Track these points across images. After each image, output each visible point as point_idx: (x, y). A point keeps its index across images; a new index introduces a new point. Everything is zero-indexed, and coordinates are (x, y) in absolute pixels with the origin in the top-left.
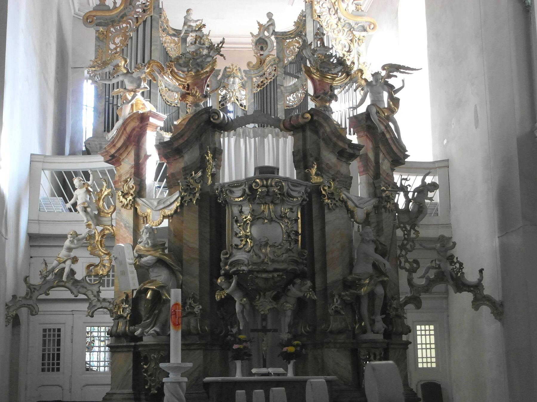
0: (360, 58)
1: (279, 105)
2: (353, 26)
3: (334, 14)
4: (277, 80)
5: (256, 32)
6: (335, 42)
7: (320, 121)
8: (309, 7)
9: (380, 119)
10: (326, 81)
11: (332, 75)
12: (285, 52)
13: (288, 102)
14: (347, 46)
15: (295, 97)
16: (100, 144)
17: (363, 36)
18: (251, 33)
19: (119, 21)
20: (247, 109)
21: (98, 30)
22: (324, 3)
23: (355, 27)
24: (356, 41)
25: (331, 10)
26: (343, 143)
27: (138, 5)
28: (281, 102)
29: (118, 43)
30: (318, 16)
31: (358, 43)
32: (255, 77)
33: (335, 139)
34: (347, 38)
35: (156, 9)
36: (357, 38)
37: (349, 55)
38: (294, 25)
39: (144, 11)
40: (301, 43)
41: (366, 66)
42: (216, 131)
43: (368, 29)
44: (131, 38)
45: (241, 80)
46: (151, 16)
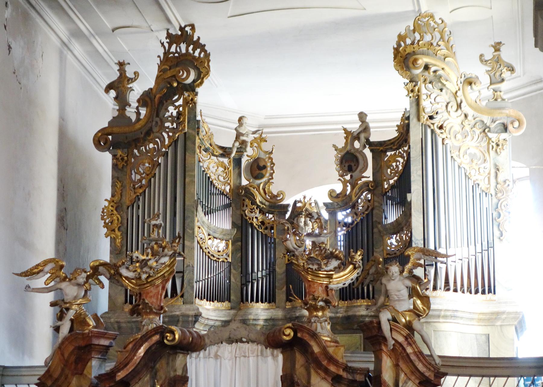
1: (376, 252)
2: (488, 125)
3: (457, 110)
4: (374, 215)
5: (341, 144)
6: (457, 153)
7: (305, 338)
8: (414, 105)
10: (319, 282)
11: (325, 273)
12: (385, 171)
13: (389, 248)
16: (117, 322)
17: (504, 140)
18: (334, 146)
19: (144, 140)
21: (116, 154)
22: (438, 95)
23: (491, 127)
25: (450, 105)
26: (335, 367)
28: (379, 248)
31: (496, 150)
33: (325, 363)
36: (495, 143)
41: (509, 185)
42: (176, 353)
43: (510, 127)
44: (160, 164)
46: (185, 133)
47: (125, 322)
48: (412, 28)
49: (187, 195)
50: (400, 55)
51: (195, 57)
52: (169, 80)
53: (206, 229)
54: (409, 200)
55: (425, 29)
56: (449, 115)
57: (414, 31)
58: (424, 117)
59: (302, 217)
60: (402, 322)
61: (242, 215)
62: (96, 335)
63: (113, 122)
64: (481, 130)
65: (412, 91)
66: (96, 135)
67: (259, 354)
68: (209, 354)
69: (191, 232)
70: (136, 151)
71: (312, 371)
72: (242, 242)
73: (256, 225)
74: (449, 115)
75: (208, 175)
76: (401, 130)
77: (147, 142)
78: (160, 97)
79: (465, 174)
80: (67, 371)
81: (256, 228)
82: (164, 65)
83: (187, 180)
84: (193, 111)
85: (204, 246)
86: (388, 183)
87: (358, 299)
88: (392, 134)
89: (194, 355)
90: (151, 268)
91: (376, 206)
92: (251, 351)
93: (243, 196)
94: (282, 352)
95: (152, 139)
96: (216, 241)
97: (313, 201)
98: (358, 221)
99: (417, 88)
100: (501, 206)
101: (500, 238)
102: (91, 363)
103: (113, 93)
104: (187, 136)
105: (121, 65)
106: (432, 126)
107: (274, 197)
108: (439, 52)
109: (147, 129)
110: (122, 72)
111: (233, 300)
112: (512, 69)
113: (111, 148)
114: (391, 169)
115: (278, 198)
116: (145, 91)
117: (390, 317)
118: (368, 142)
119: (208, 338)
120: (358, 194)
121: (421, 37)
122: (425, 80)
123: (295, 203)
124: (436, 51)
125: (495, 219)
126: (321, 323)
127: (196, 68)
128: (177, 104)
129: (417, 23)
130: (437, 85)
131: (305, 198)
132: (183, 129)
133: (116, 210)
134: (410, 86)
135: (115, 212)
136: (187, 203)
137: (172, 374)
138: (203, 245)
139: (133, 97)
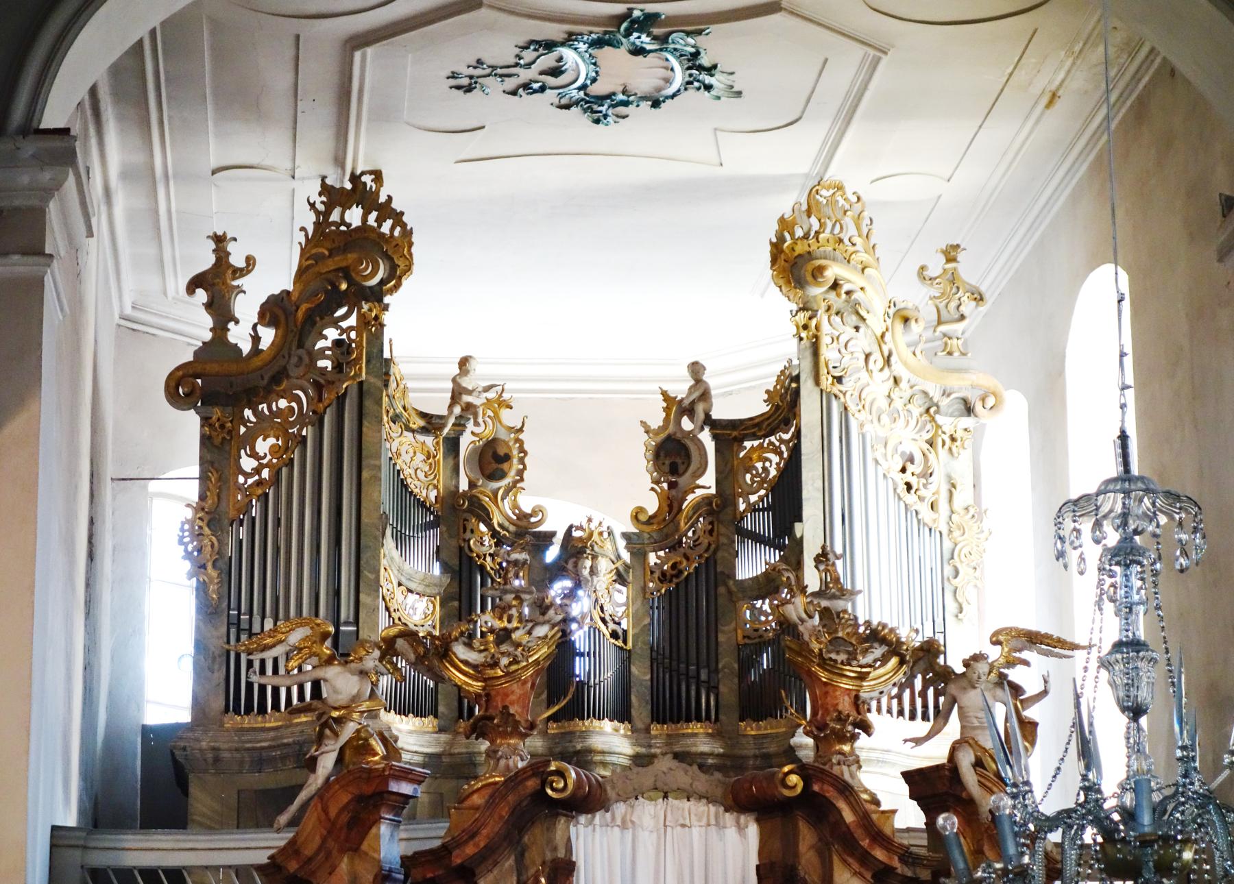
0: (956, 494)
1: (723, 632)
2: (935, 400)
3: (881, 370)
5: (656, 419)
7: (827, 795)
8: (808, 354)
9: (983, 780)
11: (859, 669)
12: (741, 481)
14: (918, 457)
15: (769, 611)
16: (214, 749)
17: (966, 430)
18: (643, 423)
20: (630, 645)
24: (944, 443)
25: (872, 359)
27: (323, 349)
29: (266, 455)
30: (834, 377)
31: (950, 449)
32: (656, 551)
33: (865, 843)
34: (917, 437)
35: (374, 362)
36: (948, 435)
37: (925, 486)
38: (765, 401)
39: (338, 367)
40: (785, 455)
42: (558, 815)
43: (978, 408)
45: (613, 562)
46: (361, 383)
47: (230, 750)
48: (805, 207)
49: (364, 504)
50: (783, 256)
51: (384, 234)
52: (331, 276)
53: (396, 572)
54: (798, 535)
55: (828, 211)
56: (871, 377)
57: (809, 213)
58: (826, 381)
59: (587, 558)
60: (991, 768)
61: (461, 549)
62: (397, 773)
63: (204, 352)
64: (922, 409)
65: (805, 327)
66: (171, 374)
67: (713, 821)
68: (613, 818)
69: (372, 576)
70: (248, 413)
71: (835, 859)
72: (460, 601)
73: (492, 568)
74: (871, 377)
75: (398, 468)
76: (777, 400)
77: (274, 396)
78: (309, 309)
79: (895, 490)
80: (331, 844)
81: (490, 575)
82: (316, 246)
83: (365, 474)
84: (376, 339)
85: (393, 606)
86: (747, 501)
87: (688, 720)
88: (754, 406)
89: (583, 819)
90: (518, 645)
91: (723, 544)
92: (696, 815)
93: (465, 511)
94: (758, 821)
95: (284, 391)
96: (412, 598)
97: (604, 528)
98: (691, 571)
99: (814, 322)
100: (959, 556)
101: (957, 616)
102: (379, 829)
103: (201, 295)
104: (365, 387)
105: (220, 240)
106: (841, 396)
107: (523, 517)
108: (853, 256)
109: (276, 368)
110: (222, 255)
111: (443, 713)
112: (979, 299)
113: (199, 404)
114: (752, 474)
115: (533, 520)
116: (273, 295)
117: (973, 759)
118: (709, 421)
119: (613, 788)
120: (691, 518)
121: (821, 226)
122: (829, 309)
123: (569, 532)
124: (849, 253)
125: (948, 579)
126: (849, 766)
127: (388, 258)
128: (344, 324)
129: (814, 197)
130: (849, 322)
131: (590, 520)
132: (358, 375)
133: (208, 525)
134: (802, 317)
135: (207, 531)
136: (365, 519)
137: (549, 856)
138: (389, 604)
139: (247, 308)
